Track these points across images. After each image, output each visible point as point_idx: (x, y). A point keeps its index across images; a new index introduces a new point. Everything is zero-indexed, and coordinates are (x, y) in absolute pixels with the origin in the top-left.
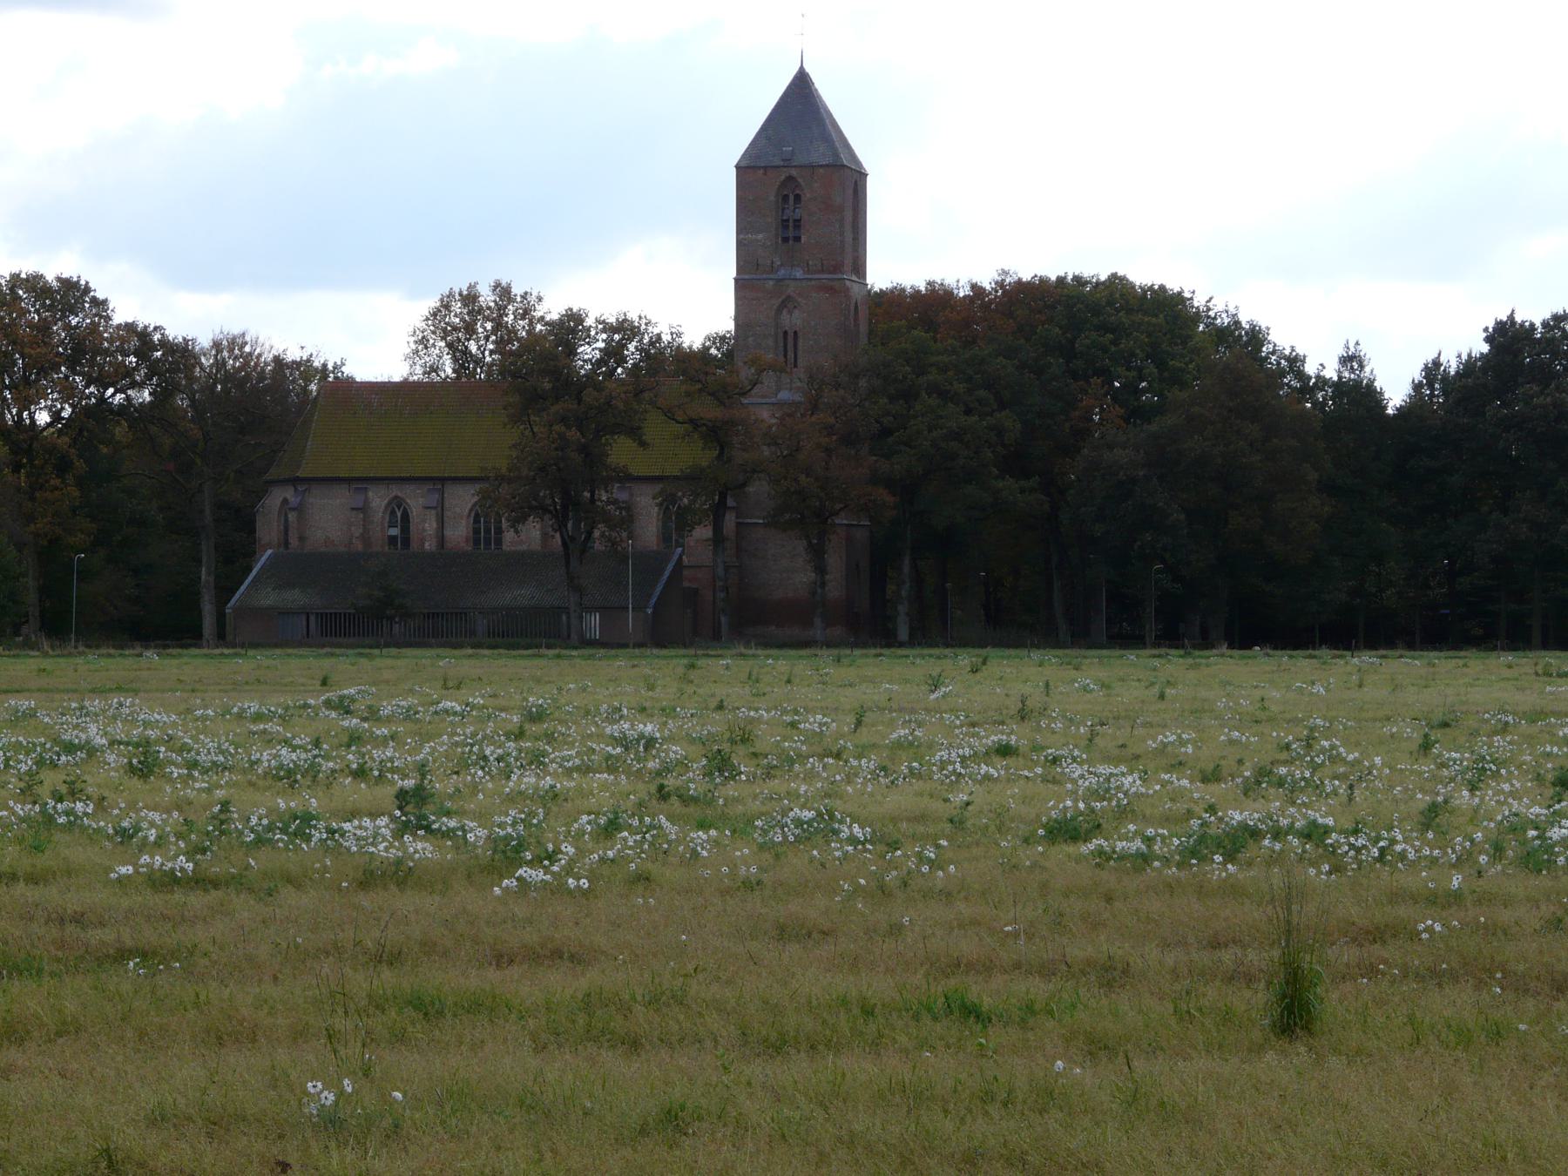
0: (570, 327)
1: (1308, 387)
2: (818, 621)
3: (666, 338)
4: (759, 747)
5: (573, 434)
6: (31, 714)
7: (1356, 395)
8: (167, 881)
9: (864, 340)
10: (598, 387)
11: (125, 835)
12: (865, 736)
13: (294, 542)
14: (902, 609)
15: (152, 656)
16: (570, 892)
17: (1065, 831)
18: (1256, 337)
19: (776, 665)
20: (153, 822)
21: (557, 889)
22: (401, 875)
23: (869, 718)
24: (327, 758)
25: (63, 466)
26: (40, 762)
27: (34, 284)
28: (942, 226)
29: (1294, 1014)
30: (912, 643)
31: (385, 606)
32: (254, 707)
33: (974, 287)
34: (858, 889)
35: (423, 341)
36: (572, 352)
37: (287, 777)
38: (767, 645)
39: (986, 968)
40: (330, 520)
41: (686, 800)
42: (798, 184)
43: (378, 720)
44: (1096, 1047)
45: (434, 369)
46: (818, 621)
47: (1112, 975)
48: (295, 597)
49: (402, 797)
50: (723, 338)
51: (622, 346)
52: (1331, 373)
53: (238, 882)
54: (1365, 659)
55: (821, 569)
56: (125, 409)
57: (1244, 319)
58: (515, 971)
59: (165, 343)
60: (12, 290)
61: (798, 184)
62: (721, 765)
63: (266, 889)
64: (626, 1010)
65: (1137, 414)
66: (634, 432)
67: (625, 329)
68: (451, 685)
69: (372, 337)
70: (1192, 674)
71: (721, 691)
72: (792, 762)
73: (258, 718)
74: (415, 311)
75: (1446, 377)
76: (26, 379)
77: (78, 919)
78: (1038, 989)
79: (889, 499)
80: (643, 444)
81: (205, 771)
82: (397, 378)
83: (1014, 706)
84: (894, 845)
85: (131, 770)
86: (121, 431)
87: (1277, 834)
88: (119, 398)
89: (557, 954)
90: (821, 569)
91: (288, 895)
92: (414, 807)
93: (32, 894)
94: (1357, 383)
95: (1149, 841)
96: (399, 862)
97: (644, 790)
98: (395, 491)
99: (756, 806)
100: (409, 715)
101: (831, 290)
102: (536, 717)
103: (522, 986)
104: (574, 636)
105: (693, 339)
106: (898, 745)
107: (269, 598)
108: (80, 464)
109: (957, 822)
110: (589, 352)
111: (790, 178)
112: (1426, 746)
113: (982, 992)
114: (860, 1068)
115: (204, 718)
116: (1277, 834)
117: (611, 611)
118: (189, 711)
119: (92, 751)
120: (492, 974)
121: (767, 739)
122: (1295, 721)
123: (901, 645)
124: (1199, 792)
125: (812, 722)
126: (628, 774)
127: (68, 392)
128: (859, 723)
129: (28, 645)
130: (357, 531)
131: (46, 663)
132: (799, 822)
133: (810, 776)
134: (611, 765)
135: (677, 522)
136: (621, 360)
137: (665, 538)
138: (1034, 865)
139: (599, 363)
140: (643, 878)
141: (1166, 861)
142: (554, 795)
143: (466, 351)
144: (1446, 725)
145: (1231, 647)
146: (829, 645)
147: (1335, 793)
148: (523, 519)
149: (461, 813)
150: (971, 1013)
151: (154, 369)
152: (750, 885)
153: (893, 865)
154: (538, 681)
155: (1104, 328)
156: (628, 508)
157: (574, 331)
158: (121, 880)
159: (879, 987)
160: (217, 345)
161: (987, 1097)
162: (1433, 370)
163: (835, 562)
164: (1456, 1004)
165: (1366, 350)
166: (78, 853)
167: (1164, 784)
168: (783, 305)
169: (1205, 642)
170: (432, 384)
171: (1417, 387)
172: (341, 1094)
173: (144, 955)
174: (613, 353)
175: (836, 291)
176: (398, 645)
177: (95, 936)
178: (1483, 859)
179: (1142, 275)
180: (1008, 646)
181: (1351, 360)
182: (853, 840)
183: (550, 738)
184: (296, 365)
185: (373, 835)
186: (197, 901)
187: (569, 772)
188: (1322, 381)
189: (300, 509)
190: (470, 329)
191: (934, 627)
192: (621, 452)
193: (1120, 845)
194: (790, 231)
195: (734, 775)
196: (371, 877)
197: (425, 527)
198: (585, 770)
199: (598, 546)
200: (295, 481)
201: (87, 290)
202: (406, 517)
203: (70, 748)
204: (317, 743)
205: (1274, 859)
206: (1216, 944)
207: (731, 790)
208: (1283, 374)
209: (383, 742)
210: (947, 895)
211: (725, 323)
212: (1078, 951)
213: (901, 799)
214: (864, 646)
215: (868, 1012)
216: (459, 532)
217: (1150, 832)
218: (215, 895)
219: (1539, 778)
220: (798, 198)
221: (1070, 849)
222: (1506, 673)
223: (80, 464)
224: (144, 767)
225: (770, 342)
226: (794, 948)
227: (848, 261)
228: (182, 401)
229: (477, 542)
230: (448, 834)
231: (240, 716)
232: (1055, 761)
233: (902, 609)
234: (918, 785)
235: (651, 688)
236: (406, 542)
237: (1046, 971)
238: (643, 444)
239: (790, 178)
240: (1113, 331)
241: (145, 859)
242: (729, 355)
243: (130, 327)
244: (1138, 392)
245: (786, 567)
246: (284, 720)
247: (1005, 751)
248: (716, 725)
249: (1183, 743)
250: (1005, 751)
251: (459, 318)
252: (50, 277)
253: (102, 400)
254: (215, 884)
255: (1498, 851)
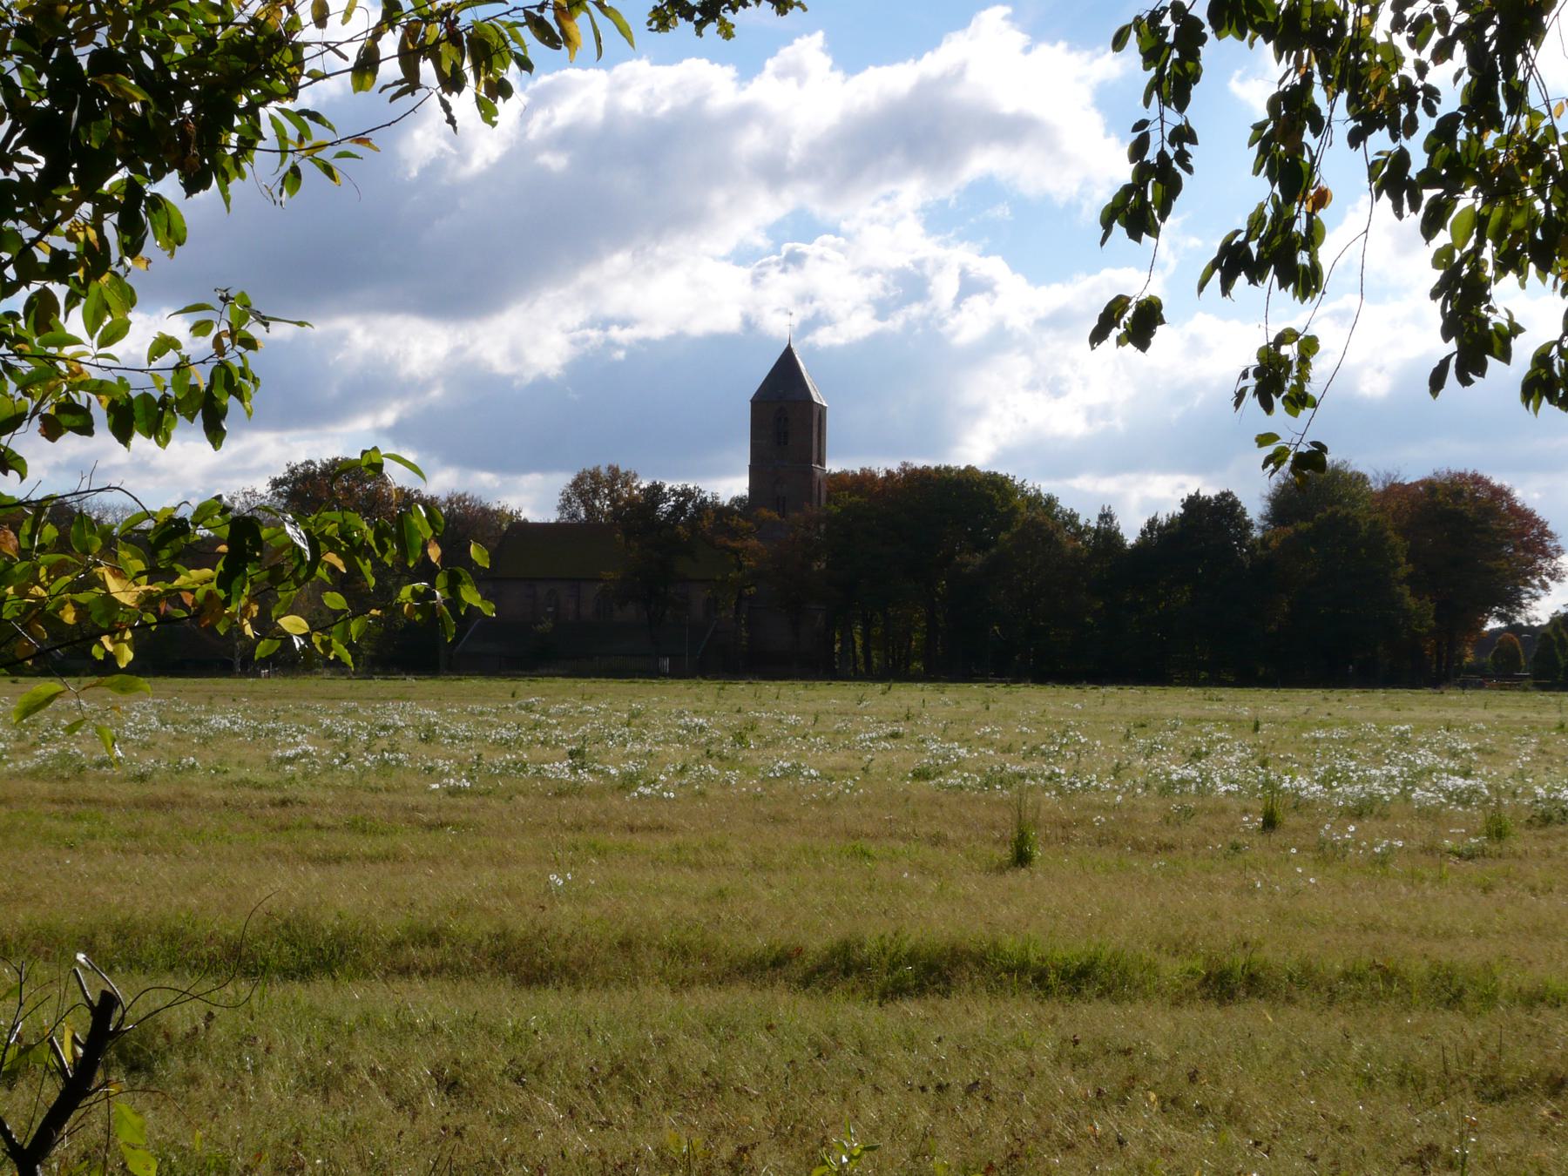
1: (1080, 532)
6: (355, 710)
7: (1107, 536)
8: (454, 792)
17: (921, 775)
18: (1051, 502)
19: (770, 688)
22: (576, 790)
23: (822, 717)
29: (1022, 858)
33: (888, 472)
35: (568, 500)
36: (655, 507)
37: (505, 745)
41: (721, 758)
43: (549, 716)
45: (574, 515)
49: (572, 754)
51: (684, 503)
52: (1093, 524)
57: (1044, 492)
62: (740, 739)
68: (587, 697)
73: (482, 713)
74: (563, 480)
75: (1160, 527)
82: (553, 521)
83: (904, 710)
84: (831, 780)
89: (661, 827)
92: (577, 756)
94: (1108, 531)
96: (575, 784)
99: (759, 762)
100: (565, 713)
102: (634, 715)
106: (838, 732)
110: (665, 507)
112: (1127, 737)
120: (628, 836)
132: (782, 769)
133: (789, 747)
134: (680, 739)
136: (684, 512)
139: (670, 514)
140: (702, 794)
142: (650, 754)
157: (655, 495)
160: (450, 500)
162: (1152, 523)
165: (1114, 510)
171: (1143, 533)
174: (679, 508)
181: (1106, 517)
182: (811, 777)
183: (646, 726)
184: (495, 512)
185: (560, 769)
187: (658, 743)
188: (1088, 529)
190: (595, 492)
193: (950, 781)
203: (384, 728)
207: (746, 753)
208: (1066, 524)
221: (924, 783)
224: (429, 737)
230: (602, 772)
234: (847, 753)
246: (496, 715)
247: (895, 735)
248: (736, 721)
249: (993, 732)
250: (895, 735)
251: (585, 487)
255: (1147, 787)
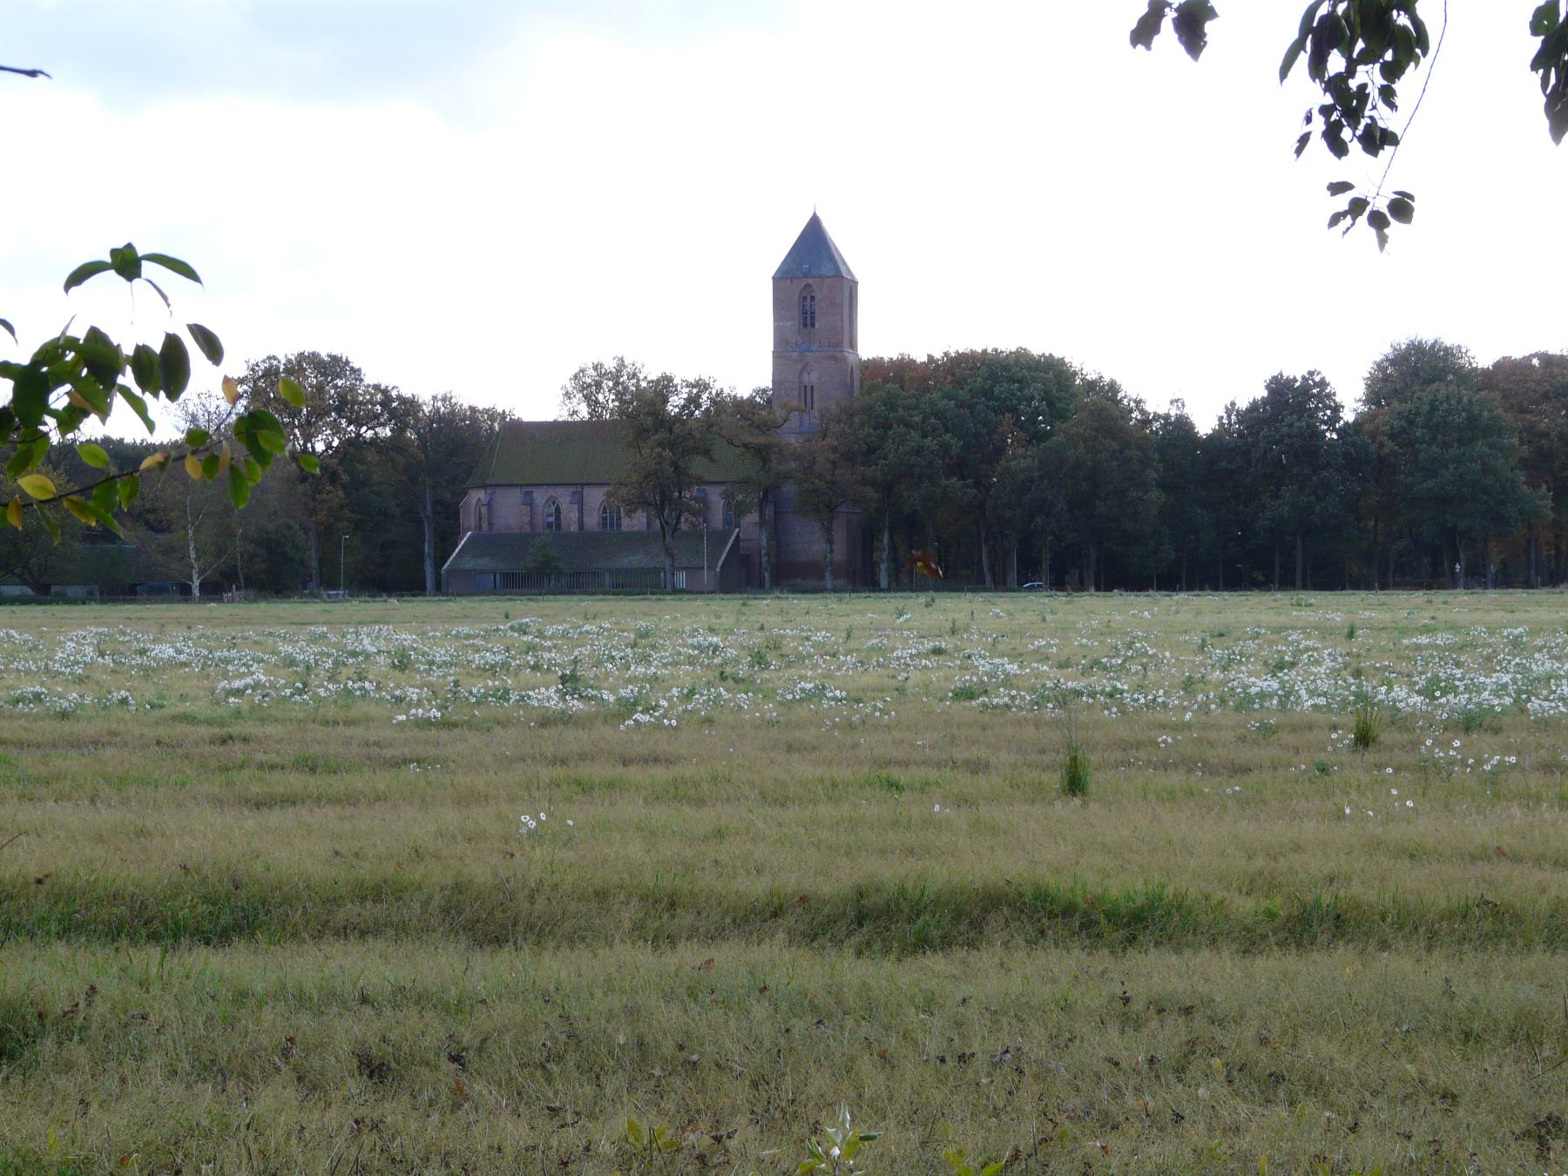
0: (664, 386)
2: (828, 576)
3: (726, 391)
4: (785, 651)
5: (667, 453)
6: (323, 636)
7: (1181, 427)
8: (427, 723)
9: (857, 392)
10: (684, 423)
11: (399, 700)
12: (852, 644)
13: (485, 526)
14: (883, 567)
15: (394, 601)
16: (666, 728)
17: (965, 694)
18: (1113, 388)
19: (797, 604)
20: (413, 694)
21: (657, 726)
22: (565, 719)
23: (856, 633)
24: (514, 658)
25: (334, 478)
26: (336, 663)
27: (313, 359)
28: (903, 322)
29: (1075, 784)
30: (889, 590)
31: (545, 567)
32: (466, 630)
34: (835, 725)
36: (666, 401)
37: (492, 670)
38: (793, 592)
39: (904, 764)
40: (510, 511)
41: (737, 681)
42: (812, 286)
43: (544, 638)
44: (962, 801)
46: (828, 576)
47: (977, 767)
48: (485, 563)
50: (764, 391)
51: (698, 396)
53: (470, 725)
54: (1182, 596)
55: (830, 542)
56: (375, 441)
58: (633, 769)
59: (399, 397)
60: (299, 363)
61: (812, 286)
62: (759, 660)
63: (484, 727)
64: (697, 785)
65: (1037, 437)
66: (707, 453)
67: (701, 386)
69: (537, 396)
70: (1068, 607)
71: (762, 619)
72: (804, 658)
73: (468, 637)
76: (309, 423)
77: (377, 744)
78: (933, 774)
79: (876, 496)
80: (712, 460)
81: (439, 667)
83: (948, 625)
85: (394, 666)
86: (371, 456)
87: (1093, 694)
88: (370, 434)
89: (656, 760)
90: (830, 542)
91: (498, 730)
92: (570, 682)
93: (349, 731)
95: (1013, 698)
96: (563, 712)
97: (712, 675)
98: (551, 492)
101: (833, 358)
102: (644, 634)
103: (634, 773)
104: (669, 588)
105: (744, 392)
106: (872, 649)
107: (469, 563)
108: (345, 478)
109: (900, 690)
110: (675, 403)
111: (808, 285)
113: (896, 774)
114: (825, 810)
115: (434, 637)
116: (1093, 694)
117: (693, 570)
118: (424, 633)
119: (368, 656)
121: (790, 646)
122: (1127, 634)
123: (882, 590)
124: (1055, 673)
125: (819, 636)
126: (702, 665)
127: (336, 429)
128: (848, 637)
129: (314, 596)
130: (527, 519)
131: (327, 606)
132: (803, 690)
133: (815, 667)
134: (691, 661)
135: (736, 511)
136: (698, 406)
137: (727, 522)
138: (943, 712)
140: (709, 721)
141: (1020, 708)
142: (655, 678)
143: (597, 402)
144: (1221, 635)
145: (1098, 589)
146: (835, 590)
147: (1136, 673)
148: (634, 511)
149: (599, 688)
150: (893, 785)
151: (393, 415)
152: (773, 724)
153: (857, 711)
154: (645, 614)
155: (1011, 380)
156: (704, 501)
157: (666, 387)
158: (400, 723)
159: (842, 773)
161: (896, 823)
163: (840, 537)
164: (1175, 779)
166: (373, 710)
167: (1032, 669)
168: (804, 368)
169: (1081, 587)
170: (575, 423)
172: (539, 821)
173: (418, 762)
174: (693, 401)
175: (839, 360)
176: (554, 594)
177: (388, 753)
178: (1213, 706)
179: (1037, 349)
180: (952, 590)
183: (653, 647)
184: (1091, 386)
185: (548, 696)
186: (444, 734)
187: (665, 666)
189: (489, 505)
190: (598, 385)
191: (904, 580)
192: (698, 465)
193: (995, 701)
194: (807, 319)
195: (768, 665)
196: (546, 721)
197: (570, 516)
198: (675, 664)
199: (684, 526)
200: (485, 487)
201: (347, 362)
202: (558, 510)
203: (354, 654)
204: (508, 650)
205: (1089, 707)
206: (1043, 751)
207: (766, 675)
208: (1131, 411)
209: (549, 650)
210: (888, 728)
211: (766, 381)
212: (960, 754)
213: (871, 678)
214: (858, 591)
215: (834, 785)
216: (592, 521)
217: (1014, 692)
218: (456, 731)
219: (1266, 663)
220: (813, 298)
222: (1274, 604)
223: (345, 478)
225: (796, 393)
226: (796, 756)
227: (846, 339)
228: (410, 434)
229: (605, 526)
231: (457, 637)
232: (969, 657)
233: (883, 567)
235: (718, 617)
236: (559, 526)
237: (939, 765)
238: (712, 460)
239: (808, 285)
240: (1019, 382)
241: (413, 711)
242: (769, 401)
243: (377, 387)
244: (1035, 422)
245: (809, 541)
247: (937, 651)
248: (758, 639)
249: (1051, 646)
250: (937, 651)
252: (324, 355)
253: (359, 435)
254: (455, 725)
